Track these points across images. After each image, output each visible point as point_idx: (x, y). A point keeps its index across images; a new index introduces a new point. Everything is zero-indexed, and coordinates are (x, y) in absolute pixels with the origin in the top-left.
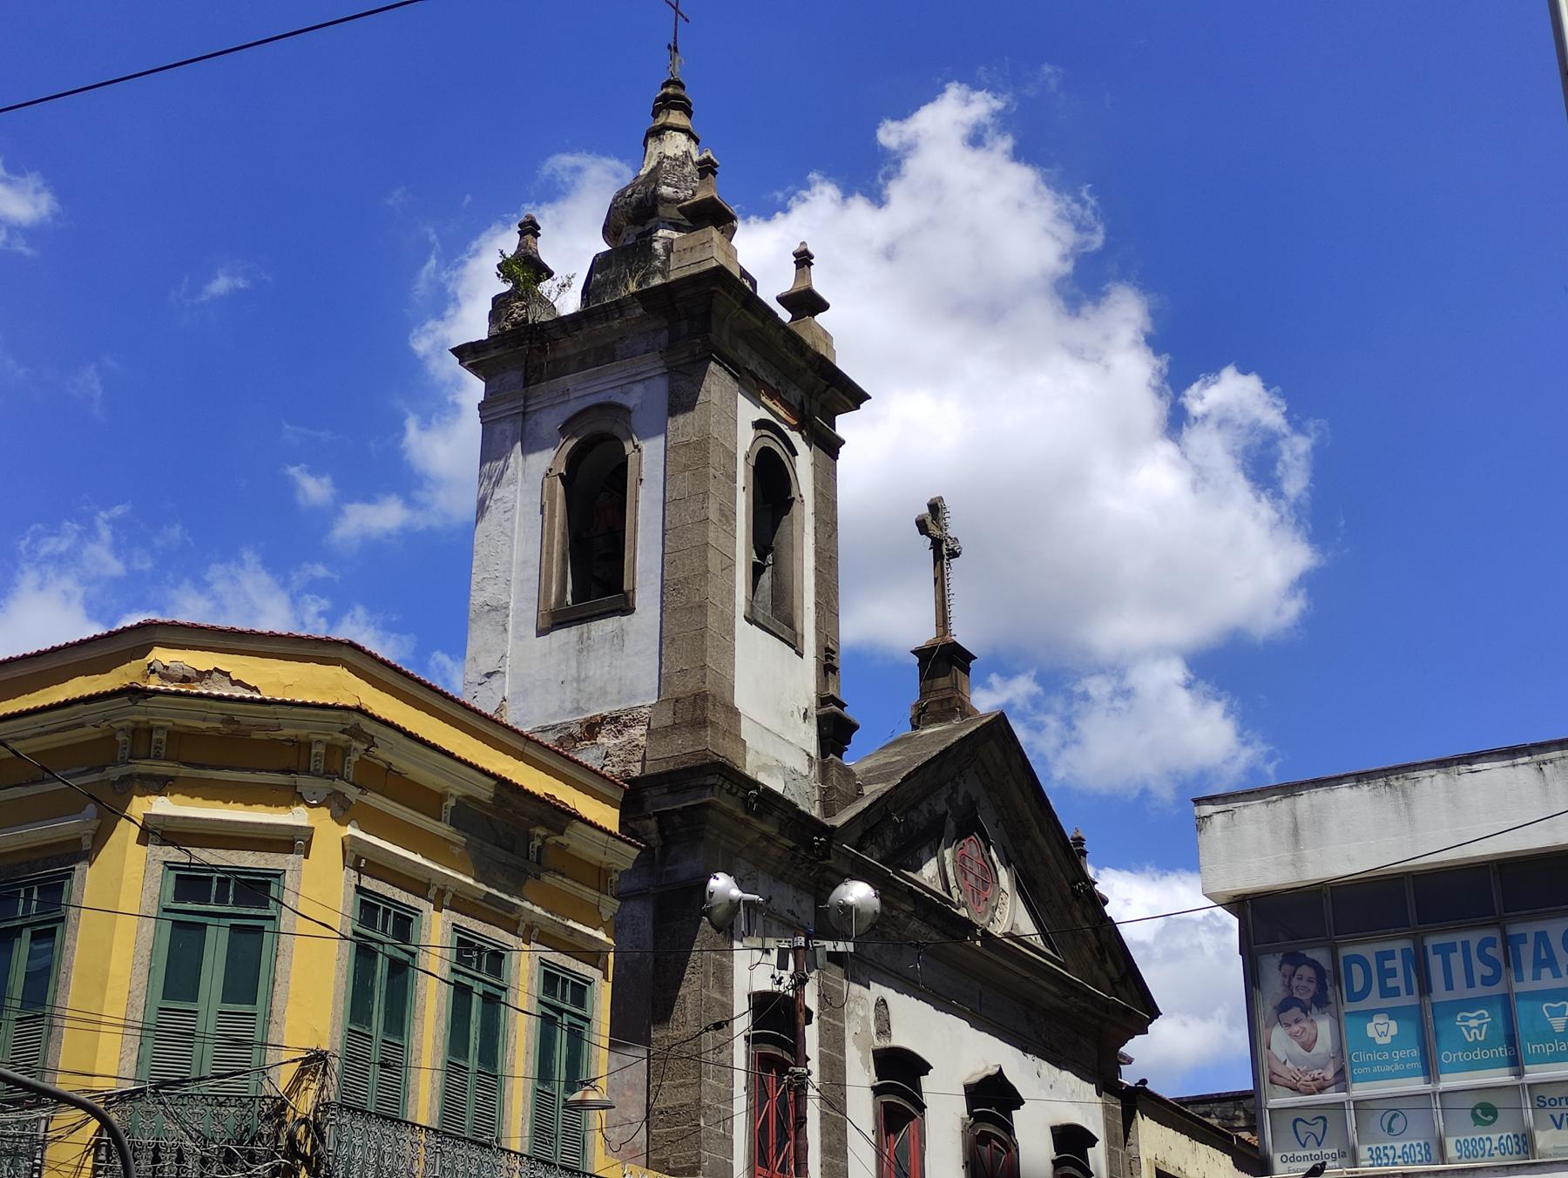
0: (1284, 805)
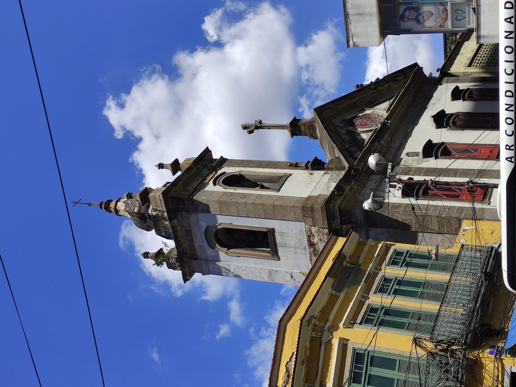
0: (351, 18)
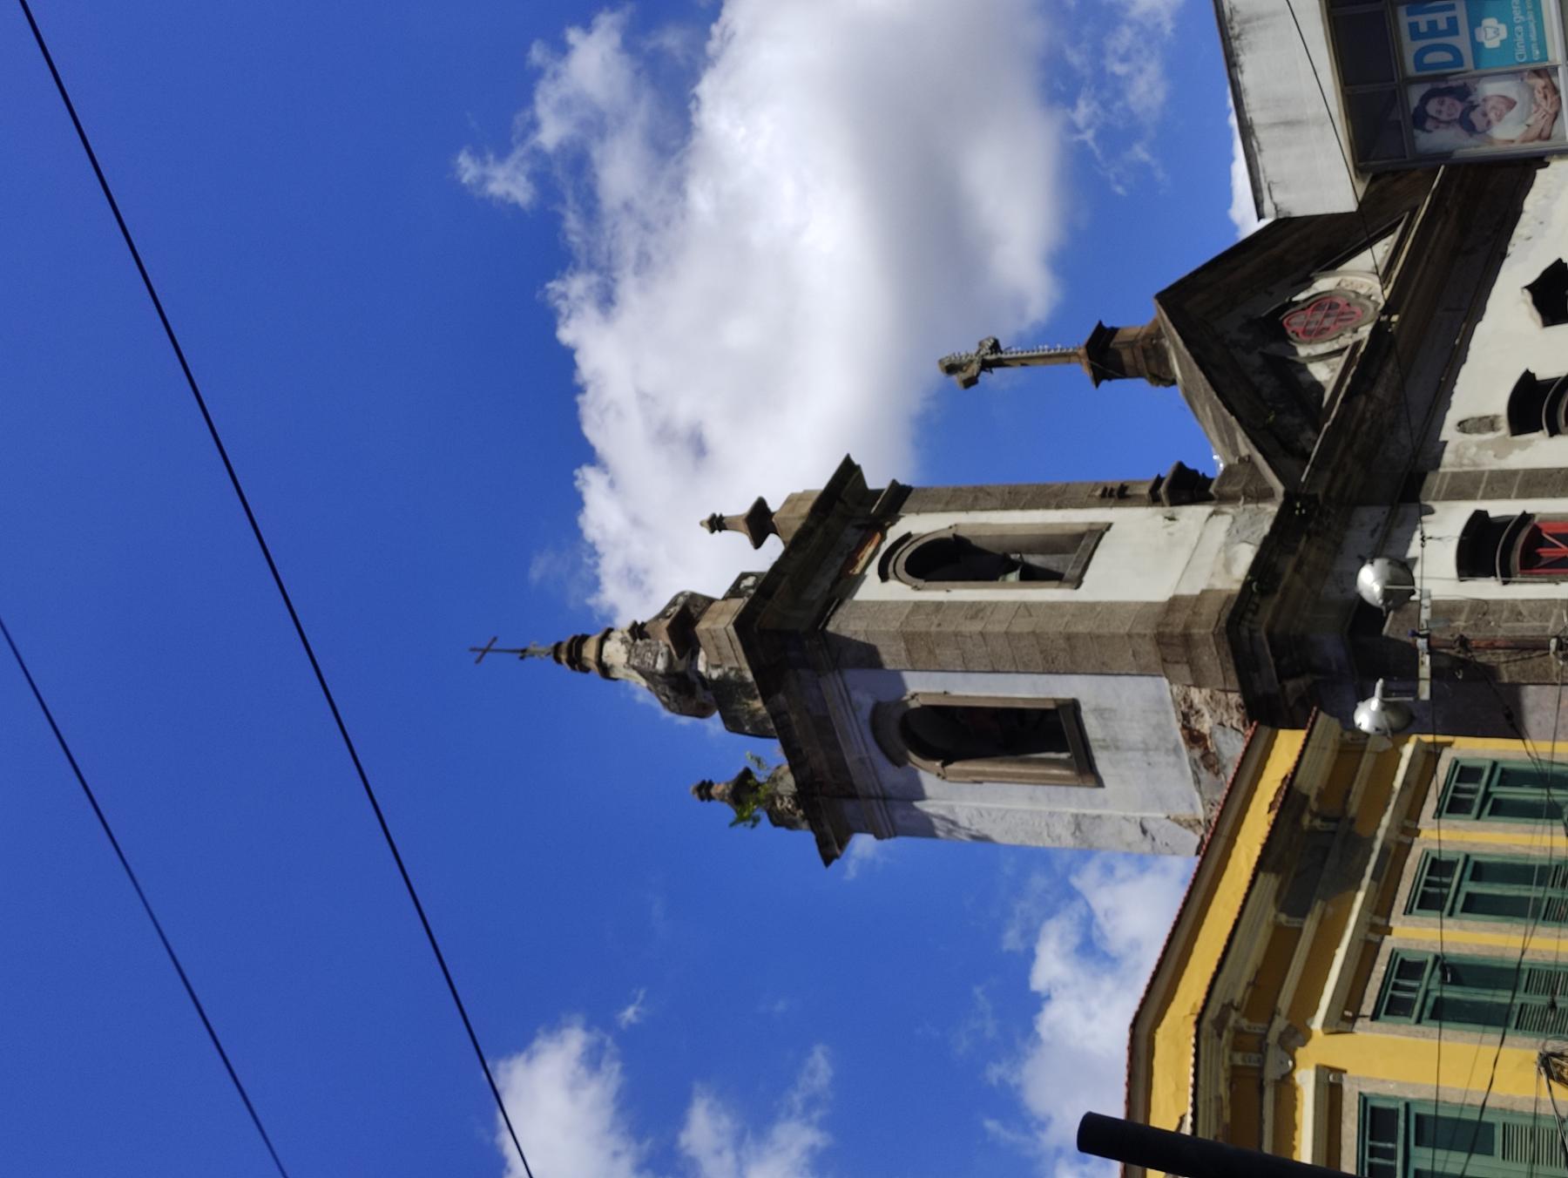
0: (1262, 135)
